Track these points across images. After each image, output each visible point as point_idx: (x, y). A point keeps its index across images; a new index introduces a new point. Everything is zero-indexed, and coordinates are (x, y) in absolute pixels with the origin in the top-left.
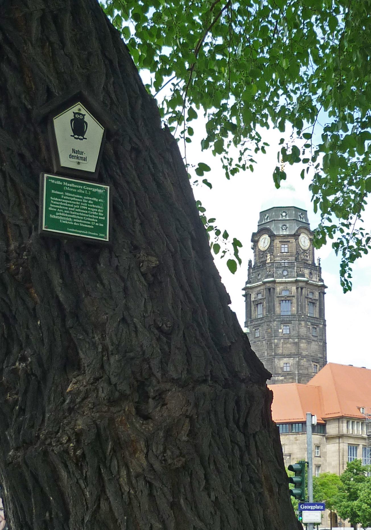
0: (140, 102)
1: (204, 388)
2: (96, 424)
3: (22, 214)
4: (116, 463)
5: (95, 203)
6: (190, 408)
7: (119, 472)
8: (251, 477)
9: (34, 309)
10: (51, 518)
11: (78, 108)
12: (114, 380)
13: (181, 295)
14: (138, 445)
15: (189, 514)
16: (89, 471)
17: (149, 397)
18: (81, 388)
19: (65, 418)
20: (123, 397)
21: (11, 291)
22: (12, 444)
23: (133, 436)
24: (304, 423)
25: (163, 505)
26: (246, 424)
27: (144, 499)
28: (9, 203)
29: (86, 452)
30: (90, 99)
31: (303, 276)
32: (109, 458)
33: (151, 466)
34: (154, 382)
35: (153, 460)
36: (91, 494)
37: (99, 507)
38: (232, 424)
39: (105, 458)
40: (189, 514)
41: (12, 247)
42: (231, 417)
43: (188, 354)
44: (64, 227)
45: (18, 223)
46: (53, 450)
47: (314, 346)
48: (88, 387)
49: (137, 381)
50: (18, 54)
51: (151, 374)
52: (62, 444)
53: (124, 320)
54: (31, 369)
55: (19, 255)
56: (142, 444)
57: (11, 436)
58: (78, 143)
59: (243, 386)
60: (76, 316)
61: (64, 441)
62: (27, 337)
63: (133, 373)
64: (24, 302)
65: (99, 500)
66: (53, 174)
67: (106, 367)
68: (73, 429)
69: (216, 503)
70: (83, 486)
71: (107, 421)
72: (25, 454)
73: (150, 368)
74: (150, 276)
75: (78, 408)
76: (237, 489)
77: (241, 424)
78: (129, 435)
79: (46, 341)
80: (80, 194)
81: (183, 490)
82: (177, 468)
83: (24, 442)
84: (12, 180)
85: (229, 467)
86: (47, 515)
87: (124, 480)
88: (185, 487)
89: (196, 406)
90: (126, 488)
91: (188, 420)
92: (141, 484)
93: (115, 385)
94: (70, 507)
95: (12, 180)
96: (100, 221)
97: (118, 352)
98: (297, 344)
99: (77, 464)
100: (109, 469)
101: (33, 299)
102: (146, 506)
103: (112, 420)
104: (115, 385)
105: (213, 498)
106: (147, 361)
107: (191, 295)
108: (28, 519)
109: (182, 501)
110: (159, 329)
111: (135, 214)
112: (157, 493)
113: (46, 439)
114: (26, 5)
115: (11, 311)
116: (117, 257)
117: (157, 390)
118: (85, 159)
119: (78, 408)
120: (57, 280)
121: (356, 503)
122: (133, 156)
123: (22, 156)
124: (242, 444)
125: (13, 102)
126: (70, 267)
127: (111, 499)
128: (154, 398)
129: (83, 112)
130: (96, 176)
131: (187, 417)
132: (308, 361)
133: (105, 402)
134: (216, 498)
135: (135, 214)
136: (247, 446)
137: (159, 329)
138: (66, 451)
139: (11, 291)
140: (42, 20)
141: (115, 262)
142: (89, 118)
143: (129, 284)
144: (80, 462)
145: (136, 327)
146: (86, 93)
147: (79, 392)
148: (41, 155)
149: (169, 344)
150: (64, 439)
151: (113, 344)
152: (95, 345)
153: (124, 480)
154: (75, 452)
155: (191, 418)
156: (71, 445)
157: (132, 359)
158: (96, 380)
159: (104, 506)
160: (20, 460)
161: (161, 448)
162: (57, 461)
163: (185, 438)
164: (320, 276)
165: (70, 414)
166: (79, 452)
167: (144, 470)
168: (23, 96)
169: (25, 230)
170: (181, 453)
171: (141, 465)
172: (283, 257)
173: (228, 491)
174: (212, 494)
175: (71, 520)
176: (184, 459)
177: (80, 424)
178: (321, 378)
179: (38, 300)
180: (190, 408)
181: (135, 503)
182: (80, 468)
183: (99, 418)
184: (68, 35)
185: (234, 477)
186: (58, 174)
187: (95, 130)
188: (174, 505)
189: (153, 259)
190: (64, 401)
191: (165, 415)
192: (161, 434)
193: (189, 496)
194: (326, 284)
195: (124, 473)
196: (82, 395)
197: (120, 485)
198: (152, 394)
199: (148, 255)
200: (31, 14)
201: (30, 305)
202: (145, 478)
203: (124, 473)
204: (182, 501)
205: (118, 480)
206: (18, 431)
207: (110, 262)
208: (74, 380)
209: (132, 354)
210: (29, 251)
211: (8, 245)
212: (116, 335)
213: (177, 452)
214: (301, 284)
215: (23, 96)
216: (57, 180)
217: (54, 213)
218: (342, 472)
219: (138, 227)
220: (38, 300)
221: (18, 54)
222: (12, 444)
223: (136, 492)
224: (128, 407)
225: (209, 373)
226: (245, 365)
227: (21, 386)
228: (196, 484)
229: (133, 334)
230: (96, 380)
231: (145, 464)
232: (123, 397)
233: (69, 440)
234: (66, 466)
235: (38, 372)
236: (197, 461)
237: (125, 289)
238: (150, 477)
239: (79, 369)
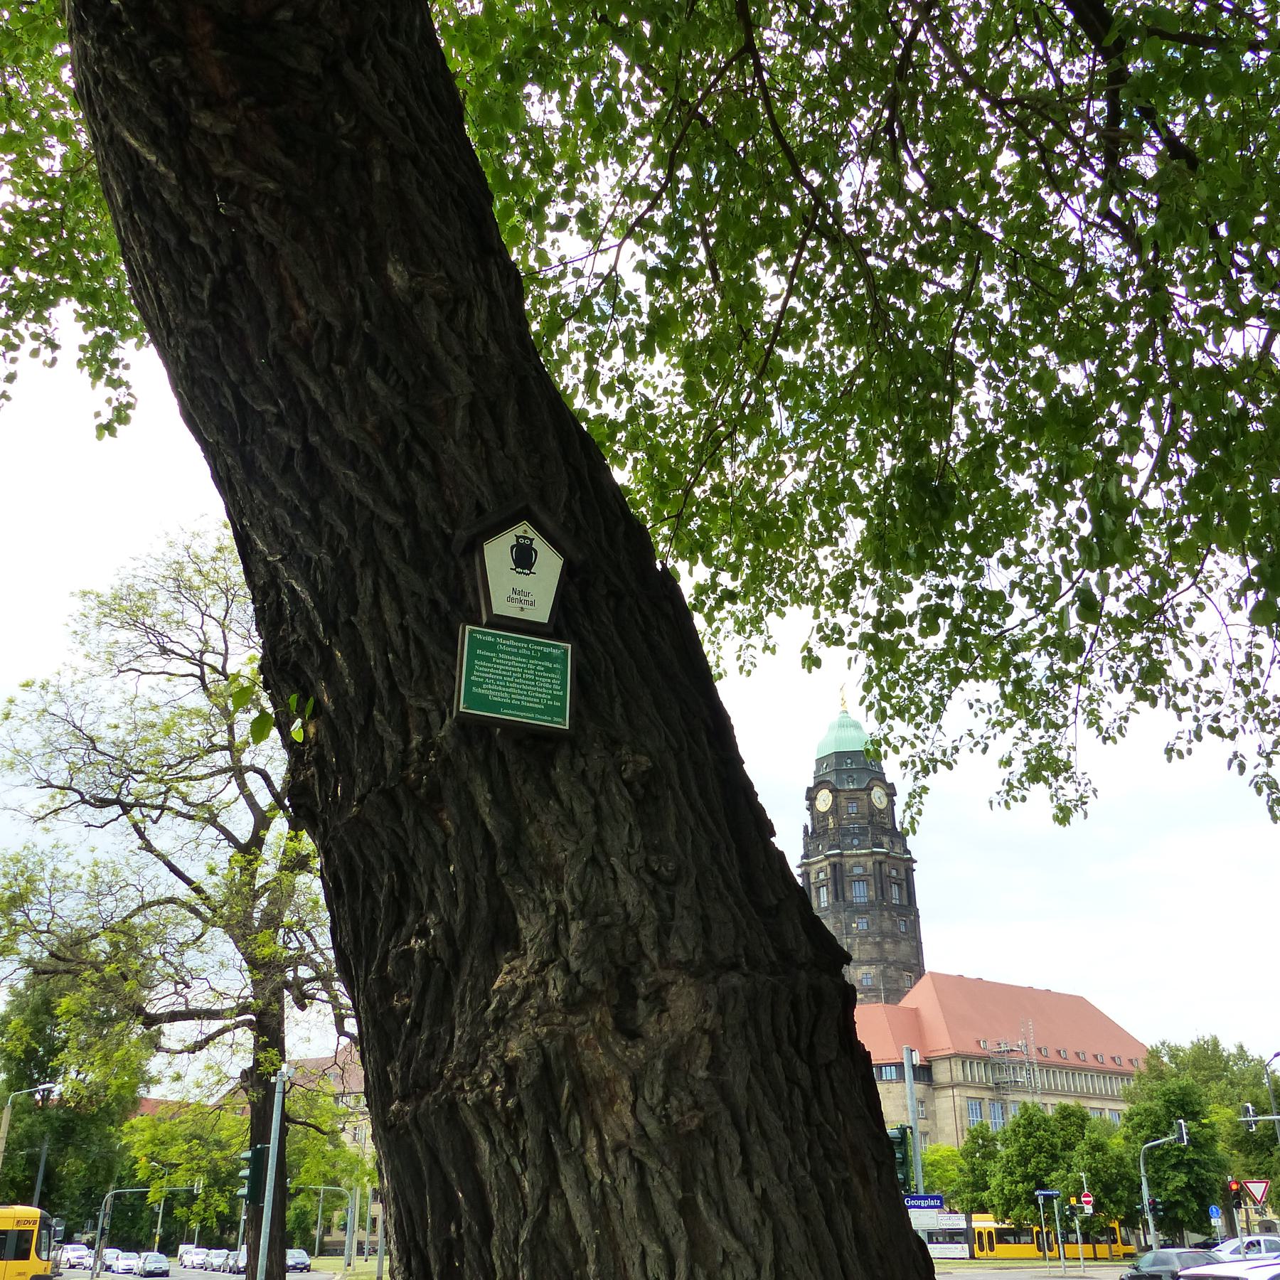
0: (622, 528)
1: (735, 979)
2: (543, 1049)
3: (431, 692)
4: (578, 1123)
5: (547, 670)
6: (709, 1015)
7: (583, 1141)
8: (826, 1149)
9: (445, 846)
10: (459, 1235)
11: (523, 529)
12: (574, 965)
13: (691, 820)
14: (618, 1089)
15: (714, 1226)
16: (528, 1139)
17: (637, 997)
18: (519, 982)
19: (489, 1037)
20: (591, 995)
21: (408, 817)
22: (396, 1088)
23: (609, 1071)
24: (900, 1066)
25: (665, 1206)
26: (811, 1046)
27: (629, 1194)
28: (412, 675)
29: (525, 1101)
30: (544, 518)
31: (881, 846)
32: (564, 1114)
33: (643, 1128)
34: (647, 968)
35: (645, 1118)
36: (532, 1185)
37: (546, 1211)
38: (786, 1046)
39: (559, 1114)
40: (714, 1226)
41: (414, 744)
42: (785, 1034)
43: (705, 920)
44: (496, 706)
45: (424, 705)
46: (465, 1100)
47: (904, 948)
48: (531, 979)
49: (617, 967)
50: (434, 458)
51: (641, 954)
52: (481, 1087)
53: (593, 860)
54: (435, 950)
55: (423, 757)
56: (625, 1086)
57: (395, 1074)
58: (522, 579)
59: (803, 975)
60: (512, 853)
61: (486, 1082)
62: (432, 892)
63: (609, 951)
64: (429, 836)
65: (548, 1198)
66: (480, 625)
67: (563, 942)
68: (501, 1058)
69: (764, 1202)
70: (518, 1169)
71: (561, 1043)
72: (418, 1107)
73: (639, 943)
74: (638, 787)
75: (512, 1018)
76: (802, 1173)
77: (803, 1045)
78: (602, 1068)
79: (461, 898)
80: (523, 656)
81: (701, 1176)
82: (690, 1132)
83: (416, 1084)
84: (418, 642)
85: (785, 1129)
86: (453, 1228)
87: (592, 1157)
88: (704, 1171)
89: (721, 1011)
90: (597, 1173)
91: (706, 1039)
92: (624, 1160)
93: (578, 973)
94: (494, 1212)
95: (418, 642)
96: (554, 698)
97: (583, 917)
98: (878, 944)
99: (507, 1126)
100: (565, 1135)
101: (444, 829)
102: (632, 1209)
103: (571, 1040)
104: (578, 973)
105: (758, 1191)
106: (635, 931)
107: (709, 820)
108: (419, 1237)
109: (700, 1198)
110: (653, 873)
111: (614, 688)
112: (654, 1183)
113: (454, 1078)
114: (448, 389)
115: (407, 850)
116: (583, 756)
117: (653, 983)
118: (532, 604)
119: (512, 1018)
120: (483, 797)
121: (986, 1194)
122: (612, 604)
123: (434, 603)
124: (807, 1083)
125: (425, 525)
126: (506, 774)
127: (569, 1195)
128: (646, 999)
129: (532, 533)
130: (551, 630)
131: (705, 1032)
132: (897, 969)
133: (559, 1005)
134: (764, 1191)
135: (614, 688)
136: (817, 1088)
137: (653, 873)
138: (488, 1101)
139: (408, 817)
140: (472, 408)
141: (580, 763)
142: (540, 544)
143: (602, 799)
144: (512, 1122)
145: (614, 872)
146: (535, 508)
147: (514, 987)
148: (464, 597)
149: (671, 900)
150: (485, 1079)
151: (574, 900)
152: (544, 905)
153: (592, 1157)
154: (504, 1102)
155: (711, 1034)
156: (498, 1088)
157: (607, 926)
158: (544, 965)
159: (555, 1210)
160: (407, 1119)
161: (659, 1092)
162: (471, 1121)
163: (702, 1074)
164: (904, 845)
165: (497, 1030)
166: (510, 1103)
167: (628, 1136)
168: (439, 516)
169: (434, 717)
170: (696, 1103)
171: (623, 1127)
172: (854, 820)
173: (785, 1176)
174: (756, 1183)
175: (495, 1239)
176: (702, 1115)
177: (515, 1049)
178: (919, 997)
179: (452, 831)
180: (709, 1015)
181: (613, 1203)
182: (513, 1134)
183: (547, 1035)
184: (511, 429)
185: (794, 1149)
186: (488, 625)
187: (549, 563)
188: (686, 1208)
189: (644, 759)
190: (488, 1005)
191: (666, 1029)
192: (660, 1065)
193: (713, 1185)
194: (914, 856)
195: (592, 1143)
196: (518, 995)
197: (586, 1167)
198: (642, 990)
199: (634, 752)
200: (455, 399)
201: (438, 838)
202: (630, 1151)
203: (592, 1143)
204: (700, 1198)
205: (582, 1157)
206: (407, 1064)
207: (572, 763)
208: (506, 967)
209: (607, 919)
210: (439, 750)
211: (407, 741)
212: (580, 886)
213: (688, 1101)
214: (879, 858)
215: (439, 516)
216: (487, 635)
217: (479, 685)
218: (962, 1144)
219: (618, 710)
220: (452, 831)
221: (434, 458)
222: (396, 1088)
223: (613, 1180)
224: (600, 1014)
225: (741, 951)
226: (803, 937)
227: (415, 980)
228: (724, 1161)
229: (610, 884)
230: (544, 965)
231: (630, 1123)
232: (591, 995)
233: (494, 1081)
234: (488, 1131)
235: (443, 952)
236: (726, 1117)
237: (597, 809)
238: (639, 1150)
239: (517, 948)
